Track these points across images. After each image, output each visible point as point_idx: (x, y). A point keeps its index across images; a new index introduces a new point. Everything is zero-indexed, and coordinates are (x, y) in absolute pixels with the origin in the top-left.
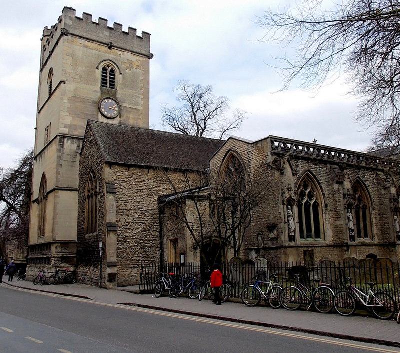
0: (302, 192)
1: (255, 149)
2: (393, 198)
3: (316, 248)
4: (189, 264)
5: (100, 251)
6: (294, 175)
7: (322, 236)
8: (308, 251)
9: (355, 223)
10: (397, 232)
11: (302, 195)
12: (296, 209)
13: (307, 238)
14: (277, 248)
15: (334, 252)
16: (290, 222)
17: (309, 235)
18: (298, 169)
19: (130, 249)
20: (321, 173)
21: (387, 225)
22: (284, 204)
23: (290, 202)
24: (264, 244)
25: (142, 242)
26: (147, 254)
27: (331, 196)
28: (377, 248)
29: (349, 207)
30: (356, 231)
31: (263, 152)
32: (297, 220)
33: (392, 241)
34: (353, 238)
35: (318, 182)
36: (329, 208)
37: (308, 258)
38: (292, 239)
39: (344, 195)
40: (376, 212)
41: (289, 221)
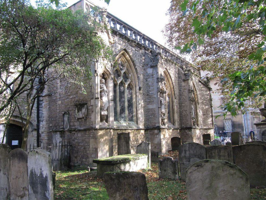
14: (85, 130)
21: (184, 112)
24: (70, 126)
37: (123, 141)
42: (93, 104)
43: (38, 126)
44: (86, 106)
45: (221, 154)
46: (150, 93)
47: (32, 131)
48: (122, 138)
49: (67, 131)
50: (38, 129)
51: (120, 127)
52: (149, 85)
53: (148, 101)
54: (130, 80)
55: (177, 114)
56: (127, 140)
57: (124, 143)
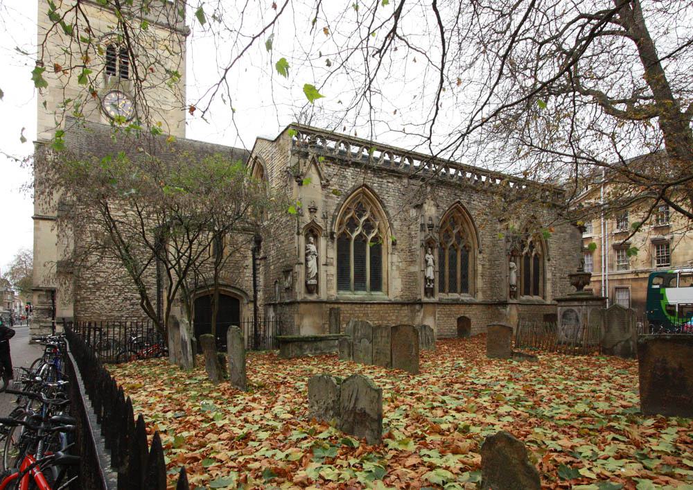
2: (511, 234)
3: (369, 306)
7: (384, 287)
9: (437, 269)
10: (511, 286)
11: (352, 224)
13: (449, 292)
15: (402, 312)
16: (310, 264)
17: (360, 283)
18: (344, 182)
19: (107, 300)
20: (390, 192)
25: (127, 290)
26: (135, 307)
27: (405, 228)
28: (480, 308)
29: (428, 245)
30: (437, 280)
33: (503, 299)
34: (429, 292)
35: (381, 202)
36: (398, 247)
40: (485, 256)
41: (307, 261)
43: (255, 297)
44: (291, 273)
45: (383, 335)
46: (413, 247)
47: (248, 303)
50: (255, 302)
54: (376, 231)
55: (483, 279)
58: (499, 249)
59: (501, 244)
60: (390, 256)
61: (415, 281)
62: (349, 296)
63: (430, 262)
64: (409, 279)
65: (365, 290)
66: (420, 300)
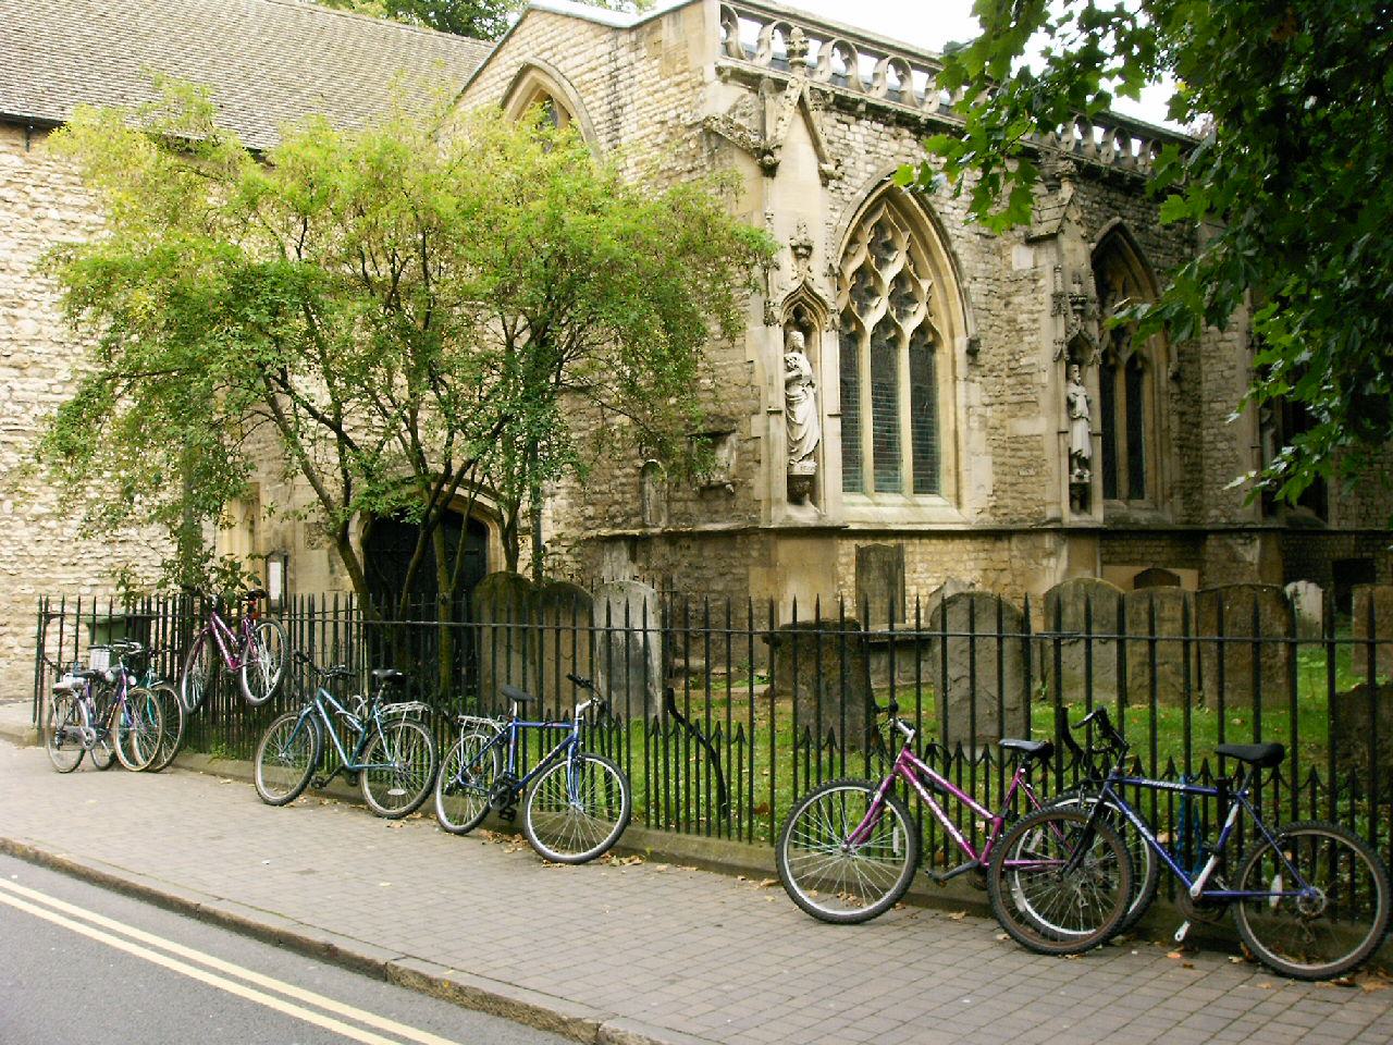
0: (861, 272)
1: (644, 52)
4: (312, 607)
5: (473, 500)
6: (826, 178)
7: (946, 482)
8: (875, 549)
9: (1098, 428)
12: (829, 346)
17: (887, 478)
19: (34, 529)
22: (769, 321)
23: (801, 315)
24: (670, 516)
27: (997, 304)
31: (679, 67)
32: (833, 401)
37: (876, 582)
38: (802, 489)
39: (1057, 297)
42: (761, 434)
48: (874, 566)
49: (658, 536)
51: (719, 71)
52: (1018, 327)
53: (1015, 399)
55: (1182, 456)
56: (891, 570)
57: (881, 585)
58: (1221, 367)
59: (1228, 354)
60: (961, 386)
61: (1035, 464)
62: (865, 510)
63: (1081, 406)
64: (1014, 457)
65: (897, 491)
66: (1058, 520)
